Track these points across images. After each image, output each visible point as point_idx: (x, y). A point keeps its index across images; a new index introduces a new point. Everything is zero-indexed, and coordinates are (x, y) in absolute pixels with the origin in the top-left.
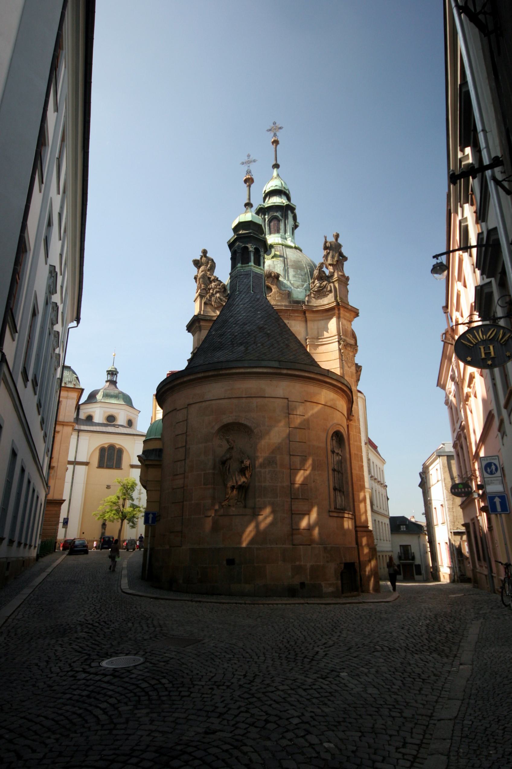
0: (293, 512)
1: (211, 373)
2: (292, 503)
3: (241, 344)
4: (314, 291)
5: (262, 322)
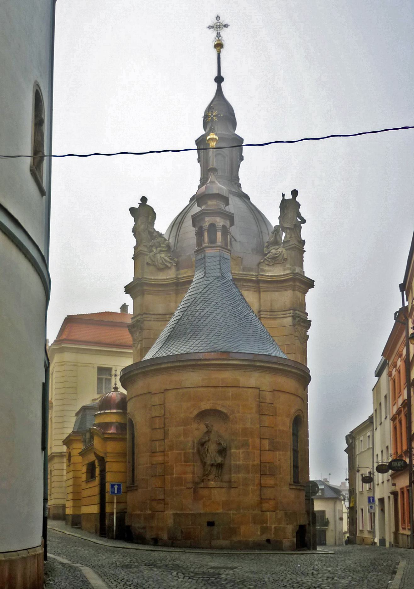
2: (261, 478)
4: (269, 258)
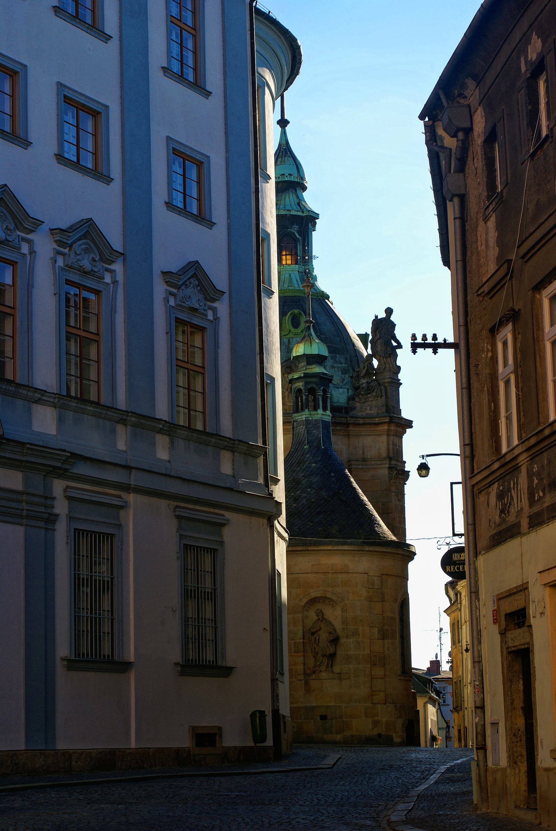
0: (372, 677)
1: (299, 548)
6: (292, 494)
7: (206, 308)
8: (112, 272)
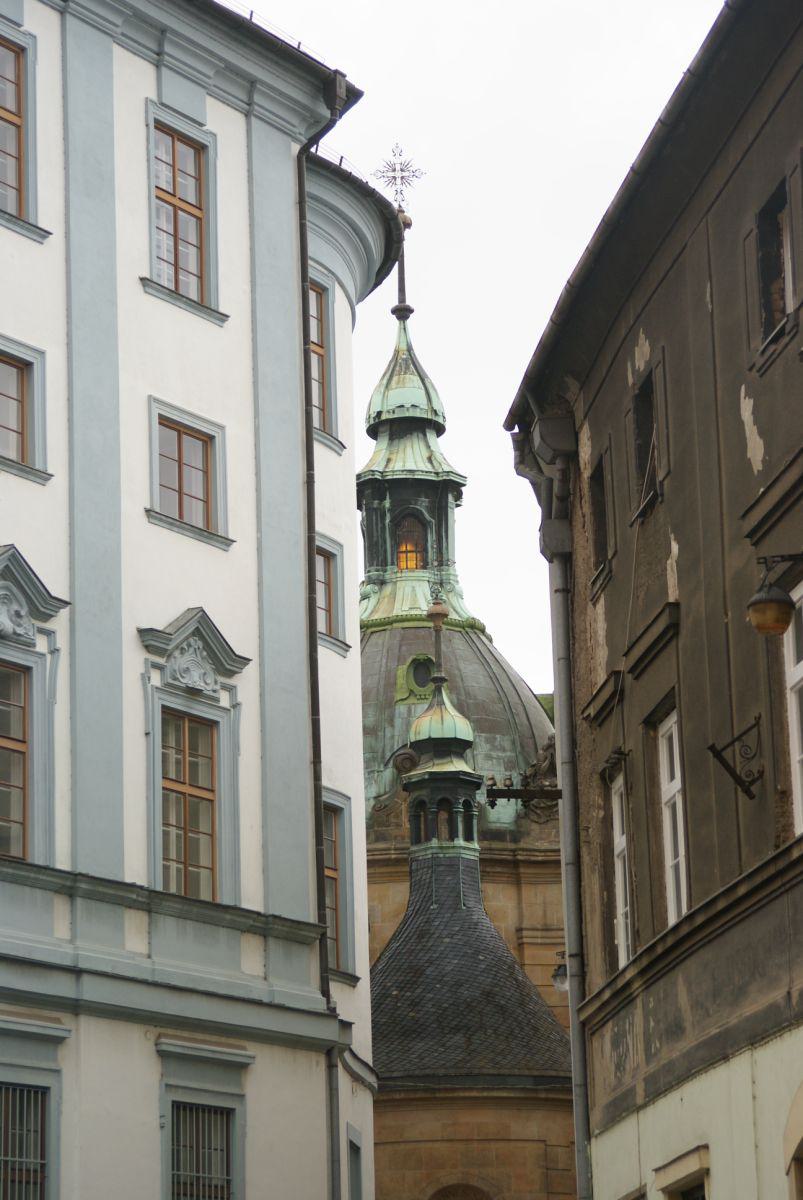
3: (456, 1030)
5: (489, 980)
6: (408, 994)
7: (218, 687)
8: (49, 633)
